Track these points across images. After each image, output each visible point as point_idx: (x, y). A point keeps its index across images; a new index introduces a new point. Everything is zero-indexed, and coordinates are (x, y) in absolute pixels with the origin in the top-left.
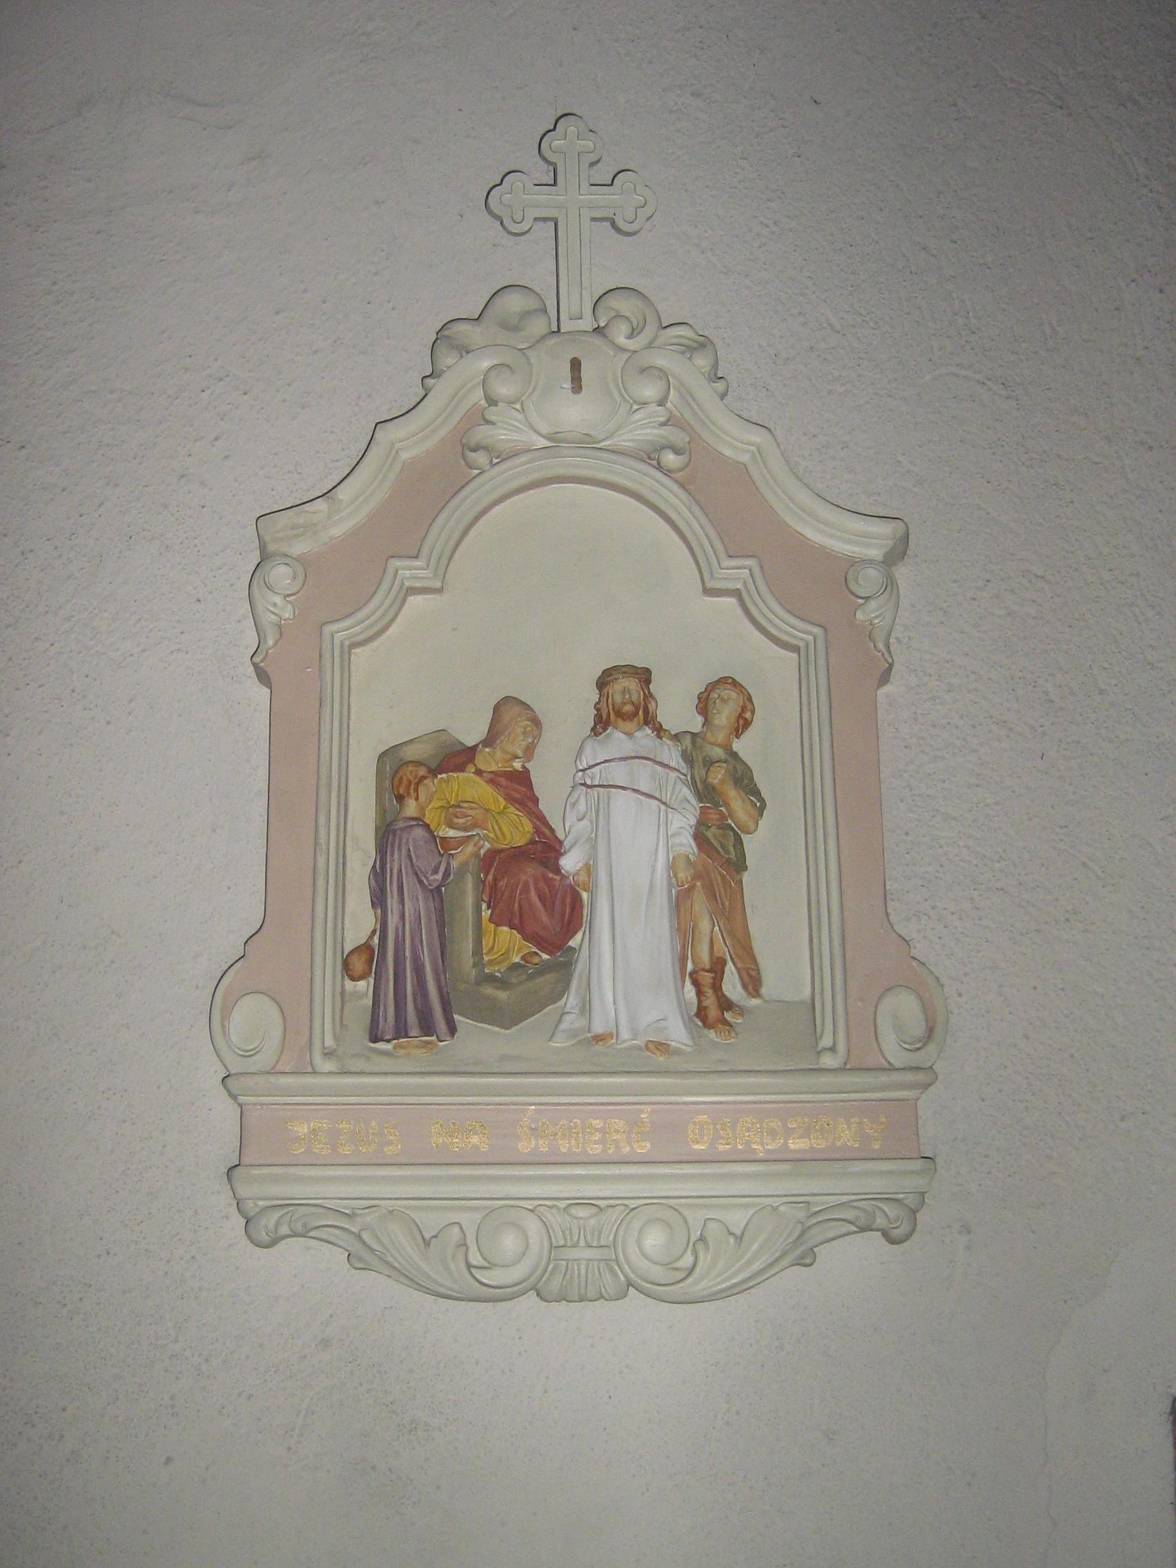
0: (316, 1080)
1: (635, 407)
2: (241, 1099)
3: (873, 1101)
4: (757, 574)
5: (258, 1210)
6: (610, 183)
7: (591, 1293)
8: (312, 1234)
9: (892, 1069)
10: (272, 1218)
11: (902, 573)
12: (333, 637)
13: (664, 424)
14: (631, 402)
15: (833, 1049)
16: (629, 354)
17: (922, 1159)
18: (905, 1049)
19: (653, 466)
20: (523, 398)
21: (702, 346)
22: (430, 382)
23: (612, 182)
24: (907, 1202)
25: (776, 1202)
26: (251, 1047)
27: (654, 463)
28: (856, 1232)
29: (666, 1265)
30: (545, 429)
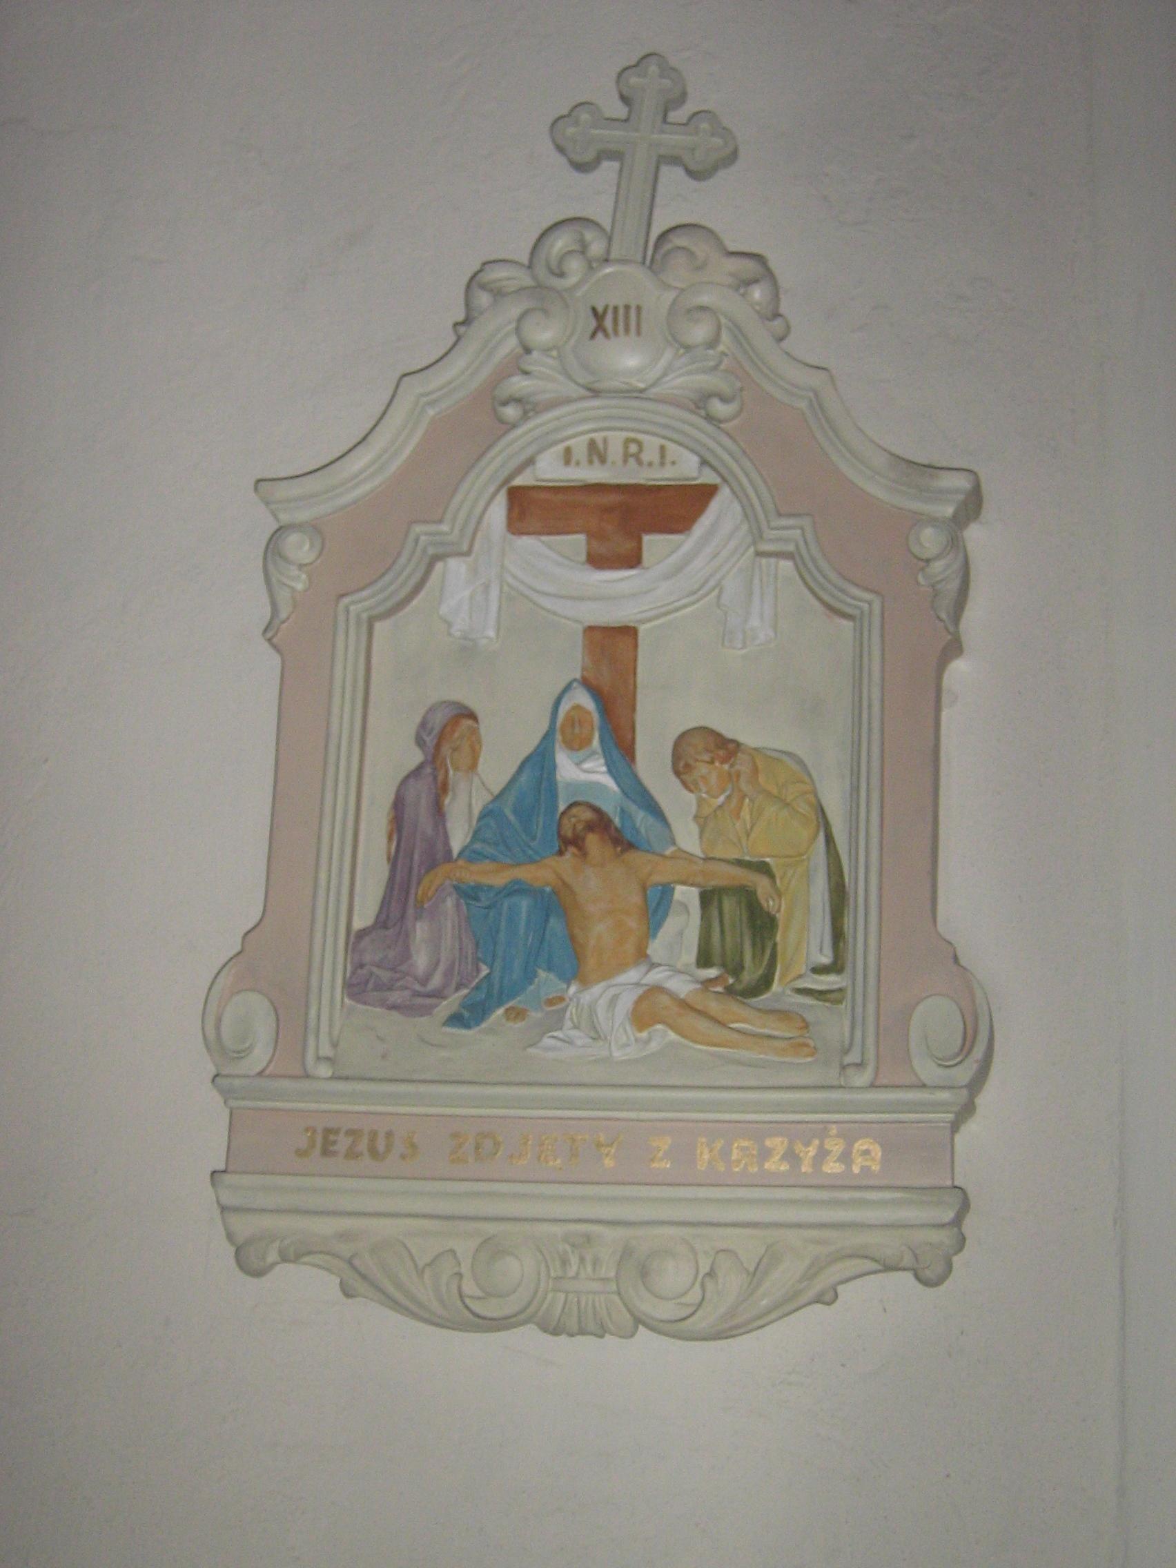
0: (673, 1094)
3: (856, 1122)
4: (810, 536)
7: (572, 1323)
11: (974, 534)
22: (462, 329)
28: (875, 1272)
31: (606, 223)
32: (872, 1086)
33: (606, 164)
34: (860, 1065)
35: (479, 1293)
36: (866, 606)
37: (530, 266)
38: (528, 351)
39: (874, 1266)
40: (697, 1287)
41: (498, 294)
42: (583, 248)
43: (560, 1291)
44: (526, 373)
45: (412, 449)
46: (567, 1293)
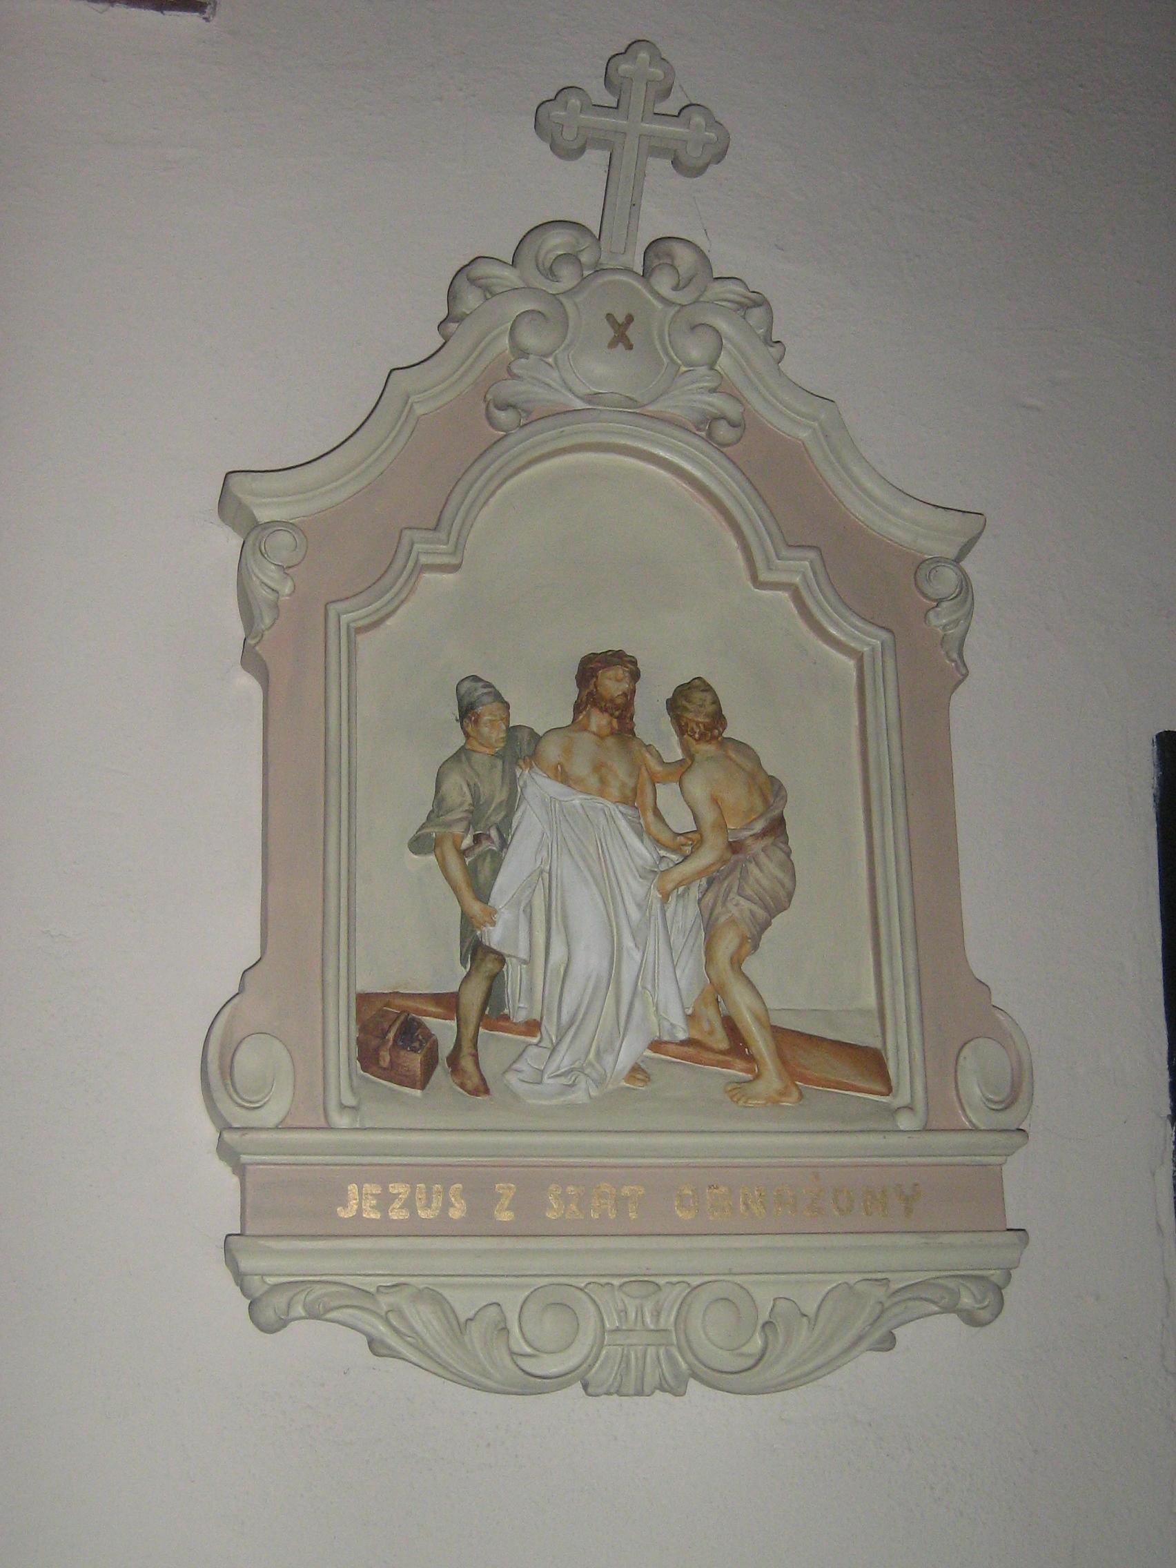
1: (684, 369)
2: (245, 1158)
5: (266, 1288)
6: (677, 114)
8: (329, 1316)
9: (975, 1129)
10: (280, 1301)
12: (339, 617)
13: (713, 391)
14: (679, 362)
15: (910, 1108)
16: (677, 308)
17: (1008, 1232)
18: (994, 1110)
19: (703, 438)
20: (557, 352)
21: (756, 304)
23: (679, 114)
24: (994, 1279)
25: (853, 1279)
26: (255, 1098)
27: (703, 434)
29: (732, 1350)
30: (583, 390)
32: (926, 1129)
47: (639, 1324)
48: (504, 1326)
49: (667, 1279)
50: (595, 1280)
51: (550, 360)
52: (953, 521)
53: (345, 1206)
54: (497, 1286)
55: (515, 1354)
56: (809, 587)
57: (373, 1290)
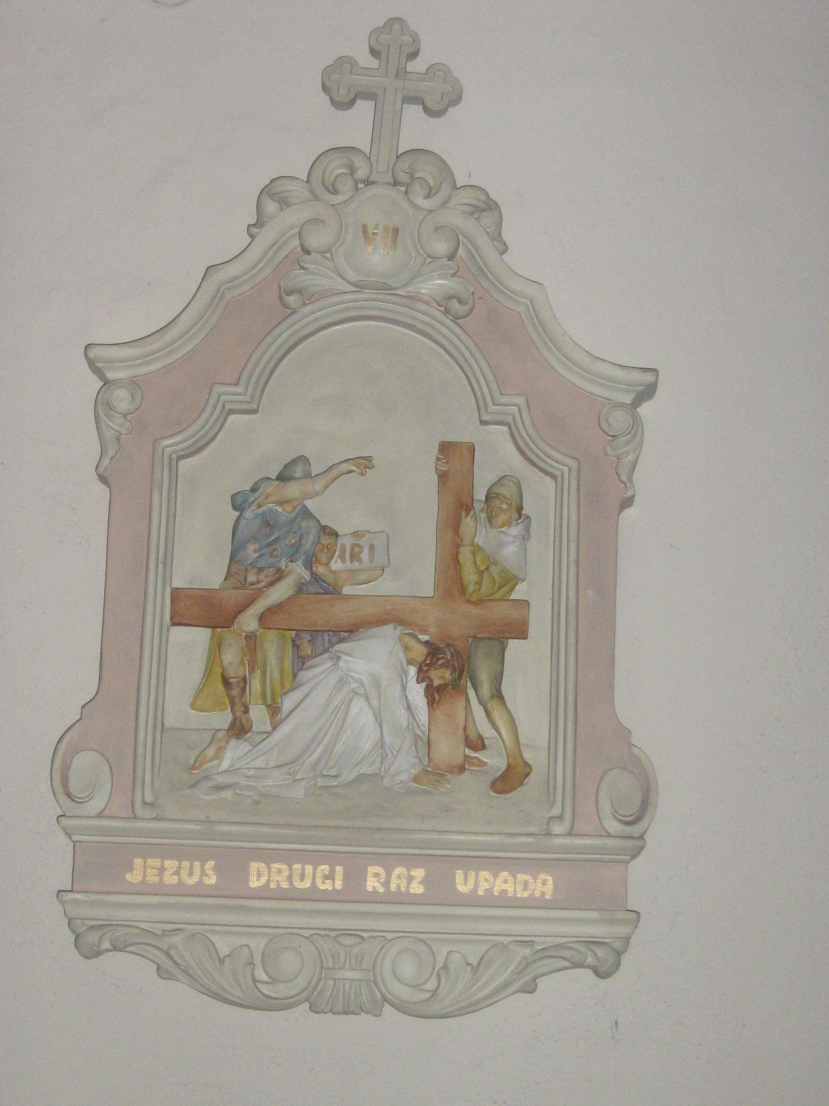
6: (425, 72)
22: (254, 230)
31: (367, 150)
32: (570, 834)
33: (360, 104)
34: (561, 817)
35: (265, 978)
36: (566, 469)
37: (308, 181)
38: (308, 252)
39: (567, 964)
40: (434, 978)
41: (284, 203)
42: (352, 170)
43: (330, 979)
44: (303, 268)
45: (402, 320)
46: (334, 979)
47: (347, 964)
48: (251, 961)
49: (369, 934)
50: (317, 932)
51: (328, 255)
52: (637, 376)
53: (213, 869)
54: (245, 933)
55: (259, 982)
56: (515, 424)
57: (159, 933)
